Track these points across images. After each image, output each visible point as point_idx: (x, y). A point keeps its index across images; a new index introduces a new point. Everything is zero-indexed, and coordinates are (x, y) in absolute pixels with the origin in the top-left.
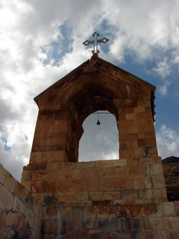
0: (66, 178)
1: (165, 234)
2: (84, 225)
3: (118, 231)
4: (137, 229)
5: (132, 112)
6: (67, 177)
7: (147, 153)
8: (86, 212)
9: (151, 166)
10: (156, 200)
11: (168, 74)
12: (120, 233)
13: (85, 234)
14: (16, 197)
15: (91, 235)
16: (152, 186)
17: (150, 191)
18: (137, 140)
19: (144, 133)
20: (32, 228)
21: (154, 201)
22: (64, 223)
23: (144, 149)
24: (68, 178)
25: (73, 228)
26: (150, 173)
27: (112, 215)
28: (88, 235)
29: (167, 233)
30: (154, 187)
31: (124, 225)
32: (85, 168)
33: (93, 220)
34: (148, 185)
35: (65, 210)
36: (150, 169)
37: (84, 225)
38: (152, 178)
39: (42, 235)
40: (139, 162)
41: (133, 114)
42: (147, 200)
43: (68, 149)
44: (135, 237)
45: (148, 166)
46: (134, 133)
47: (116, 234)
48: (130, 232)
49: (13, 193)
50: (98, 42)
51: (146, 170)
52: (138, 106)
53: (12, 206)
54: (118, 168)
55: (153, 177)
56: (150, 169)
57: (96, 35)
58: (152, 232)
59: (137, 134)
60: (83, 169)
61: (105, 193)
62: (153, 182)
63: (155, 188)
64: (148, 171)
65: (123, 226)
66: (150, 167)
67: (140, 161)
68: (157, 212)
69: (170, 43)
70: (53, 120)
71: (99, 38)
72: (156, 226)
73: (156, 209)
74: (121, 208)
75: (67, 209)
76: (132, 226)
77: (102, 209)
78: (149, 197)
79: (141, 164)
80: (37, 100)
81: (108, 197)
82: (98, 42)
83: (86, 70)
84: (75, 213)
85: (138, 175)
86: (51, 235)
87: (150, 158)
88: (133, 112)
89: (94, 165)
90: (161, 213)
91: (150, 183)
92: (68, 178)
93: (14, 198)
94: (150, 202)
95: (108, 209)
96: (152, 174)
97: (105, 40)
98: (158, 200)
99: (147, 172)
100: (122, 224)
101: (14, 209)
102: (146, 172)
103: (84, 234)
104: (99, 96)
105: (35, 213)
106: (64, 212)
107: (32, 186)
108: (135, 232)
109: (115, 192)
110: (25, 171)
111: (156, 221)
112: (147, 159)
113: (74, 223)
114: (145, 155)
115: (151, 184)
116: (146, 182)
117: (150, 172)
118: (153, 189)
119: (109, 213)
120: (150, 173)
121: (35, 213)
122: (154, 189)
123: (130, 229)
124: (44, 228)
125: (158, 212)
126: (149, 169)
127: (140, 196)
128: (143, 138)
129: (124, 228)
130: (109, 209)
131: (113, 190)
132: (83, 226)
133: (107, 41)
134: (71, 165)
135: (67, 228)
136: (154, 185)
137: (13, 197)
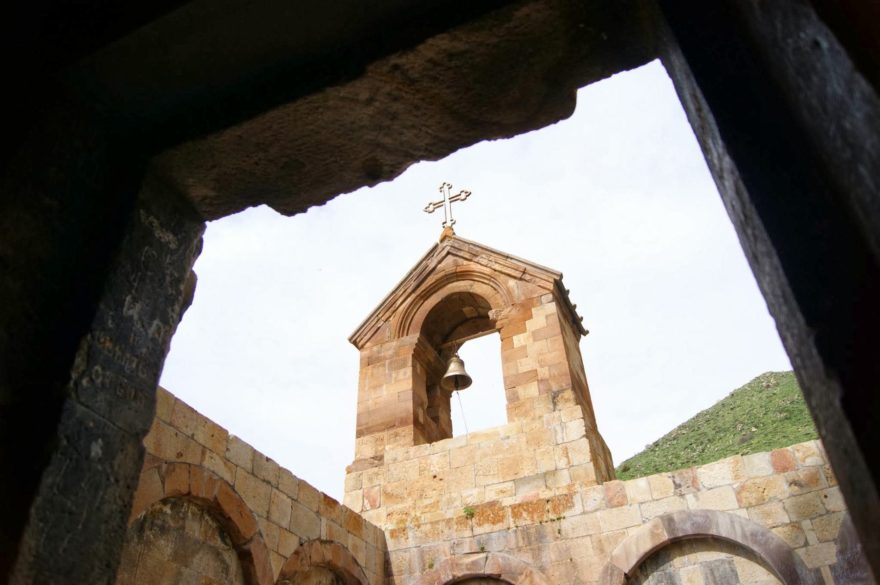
1: (590, 543)
2: (454, 550)
3: (510, 551)
6: (421, 471)
7: (555, 404)
8: (455, 527)
10: (575, 487)
12: (514, 554)
13: (457, 564)
14: (322, 518)
15: (467, 565)
17: (565, 472)
19: (547, 367)
22: (422, 553)
24: (424, 474)
25: (436, 558)
27: (499, 524)
28: (462, 567)
29: (593, 541)
30: (571, 464)
31: (520, 538)
32: (449, 450)
34: (562, 461)
35: (420, 529)
36: (562, 432)
37: (454, 550)
38: (566, 448)
40: (543, 422)
43: (591, 427)
45: (559, 429)
46: (529, 370)
47: (508, 556)
49: (318, 512)
51: (556, 436)
53: (319, 533)
56: (562, 432)
57: (446, 188)
58: (567, 543)
61: (489, 488)
62: (570, 455)
64: (559, 437)
65: (518, 541)
66: (563, 429)
68: (574, 506)
70: (387, 372)
71: (454, 192)
73: (573, 502)
75: (423, 528)
76: (533, 539)
79: (545, 426)
84: (436, 532)
86: (402, 576)
88: (525, 331)
91: (563, 458)
92: (424, 474)
93: (321, 520)
94: (565, 492)
95: (490, 516)
98: (579, 486)
99: (557, 438)
100: (516, 537)
103: (455, 565)
104: (468, 308)
105: (366, 542)
107: (365, 499)
108: (539, 549)
109: (506, 485)
110: (250, 453)
115: (566, 459)
116: (556, 458)
117: (563, 437)
119: (493, 523)
121: (366, 542)
124: (389, 566)
125: (576, 507)
126: (560, 432)
127: (548, 485)
129: (521, 544)
130: (493, 516)
135: (427, 561)
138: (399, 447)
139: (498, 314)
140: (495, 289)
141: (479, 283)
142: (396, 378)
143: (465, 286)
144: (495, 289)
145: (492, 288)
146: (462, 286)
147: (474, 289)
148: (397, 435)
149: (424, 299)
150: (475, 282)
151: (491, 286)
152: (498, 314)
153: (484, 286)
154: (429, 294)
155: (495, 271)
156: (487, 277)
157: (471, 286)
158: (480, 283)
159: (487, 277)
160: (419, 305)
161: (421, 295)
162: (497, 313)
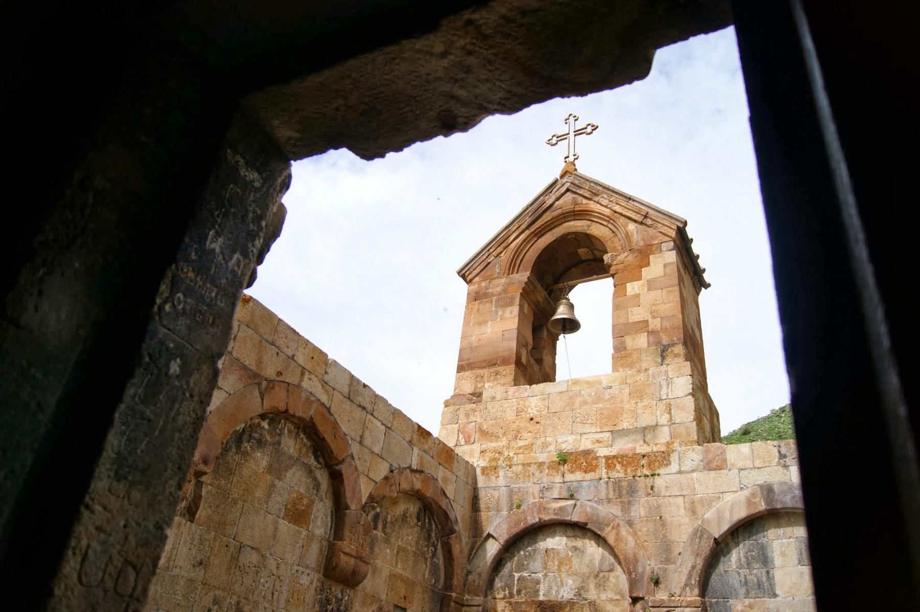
0: (517, 416)
3: (600, 501)
4: (632, 496)
5: (639, 278)
6: (519, 412)
7: (663, 358)
9: (669, 381)
11: (800, 492)
15: (555, 510)
18: (646, 333)
20: (453, 501)
21: (671, 446)
25: (524, 499)
26: (667, 395)
27: (591, 473)
30: (674, 421)
31: (611, 490)
32: (549, 394)
33: (558, 485)
35: (511, 470)
36: (668, 388)
38: (670, 404)
39: (475, 513)
40: (648, 375)
41: (641, 282)
42: (659, 446)
44: (629, 511)
48: (621, 502)
52: (651, 263)
56: (668, 388)
57: (572, 119)
61: (585, 436)
66: (668, 384)
69: (792, 423)
72: (667, 490)
74: (606, 461)
75: (514, 468)
77: (573, 464)
78: (664, 441)
80: (464, 274)
81: (586, 444)
85: (645, 400)
87: (669, 366)
89: (566, 386)
93: (413, 449)
94: (663, 449)
96: (670, 397)
99: (662, 393)
100: (607, 489)
102: (660, 394)
107: (460, 434)
108: (629, 503)
109: (602, 435)
111: (668, 481)
112: (664, 367)
113: (527, 492)
114: (659, 360)
118: (672, 424)
120: (667, 395)
121: (457, 476)
122: (673, 426)
128: (658, 327)
129: (611, 495)
131: (598, 431)
132: (541, 495)
136: (673, 418)
137: (411, 447)
138: (499, 386)
139: (614, 259)
140: (613, 232)
141: (597, 224)
143: (582, 226)
144: (613, 232)
145: (610, 231)
146: (577, 226)
147: (591, 230)
148: (497, 373)
150: (594, 223)
151: (610, 229)
152: (614, 259)
153: (602, 228)
155: (615, 212)
156: (606, 218)
157: (589, 226)
158: (598, 224)
159: (606, 218)
160: (533, 242)
161: (535, 233)
162: (613, 257)
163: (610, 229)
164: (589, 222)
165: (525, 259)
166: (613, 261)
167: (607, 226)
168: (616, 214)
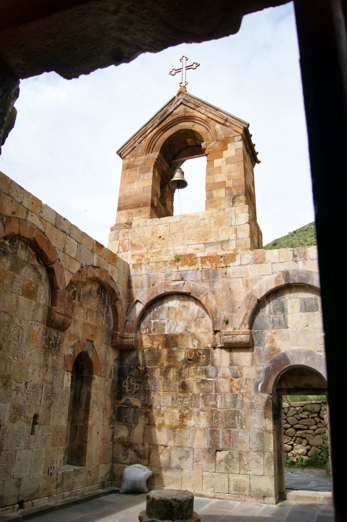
1: (242, 281)
3: (197, 281)
6: (153, 233)
8: (169, 265)
9: (236, 216)
13: (167, 285)
15: (173, 286)
16: (237, 237)
23: (231, 198)
31: (204, 275)
32: (170, 223)
36: (235, 219)
38: (236, 228)
41: (222, 159)
45: (233, 217)
48: (209, 282)
49: (92, 251)
50: (186, 69)
51: (231, 221)
54: (203, 221)
55: (238, 227)
56: (235, 219)
59: (225, 182)
60: (168, 224)
63: (238, 239)
66: (236, 217)
67: (226, 211)
71: (189, 63)
76: (211, 276)
81: (190, 251)
82: (186, 69)
83: (19, 190)
90: (239, 262)
97: (195, 66)
101: (95, 265)
105: (119, 269)
106: (148, 268)
108: (213, 282)
112: (234, 208)
116: (230, 233)
121: (119, 269)
123: (209, 278)
129: (204, 278)
133: (197, 66)
134: (157, 221)
140: (207, 129)
142: (143, 178)
143: (189, 125)
144: (207, 129)
149: (164, 131)
151: (206, 128)
153: (201, 127)
154: (167, 129)
155: (209, 117)
156: (203, 121)
157: (193, 126)
159: (203, 121)
163: (206, 128)
164: (193, 123)
165: (156, 145)
166: (207, 146)
167: (204, 126)
168: (209, 119)
